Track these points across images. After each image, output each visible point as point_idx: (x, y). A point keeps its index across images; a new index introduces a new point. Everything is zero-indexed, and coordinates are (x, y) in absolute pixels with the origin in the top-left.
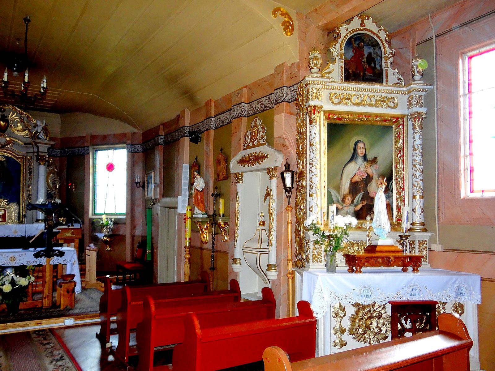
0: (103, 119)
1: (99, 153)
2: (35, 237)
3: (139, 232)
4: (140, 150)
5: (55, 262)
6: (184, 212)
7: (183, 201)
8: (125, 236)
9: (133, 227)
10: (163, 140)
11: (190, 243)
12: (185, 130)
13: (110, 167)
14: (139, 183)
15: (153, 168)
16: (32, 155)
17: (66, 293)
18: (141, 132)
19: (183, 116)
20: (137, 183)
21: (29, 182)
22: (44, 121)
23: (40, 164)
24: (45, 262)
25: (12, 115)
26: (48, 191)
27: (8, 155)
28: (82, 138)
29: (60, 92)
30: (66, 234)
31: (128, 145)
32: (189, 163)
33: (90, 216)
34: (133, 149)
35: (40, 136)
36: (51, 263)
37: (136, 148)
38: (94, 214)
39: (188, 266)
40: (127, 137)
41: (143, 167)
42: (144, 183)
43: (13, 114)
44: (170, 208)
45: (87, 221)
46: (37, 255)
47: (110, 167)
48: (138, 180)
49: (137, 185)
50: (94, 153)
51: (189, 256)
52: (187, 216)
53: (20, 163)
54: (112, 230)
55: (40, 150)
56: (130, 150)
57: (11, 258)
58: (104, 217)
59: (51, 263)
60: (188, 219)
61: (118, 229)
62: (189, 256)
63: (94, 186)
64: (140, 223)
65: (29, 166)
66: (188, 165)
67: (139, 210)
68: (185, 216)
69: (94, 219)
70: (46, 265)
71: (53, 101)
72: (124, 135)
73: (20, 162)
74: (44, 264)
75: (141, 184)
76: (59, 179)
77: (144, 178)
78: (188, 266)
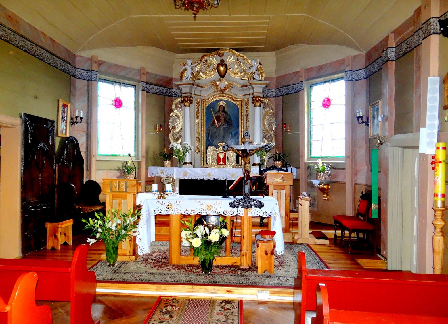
0: (316, 46)
1: (315, 89)
2: (235, 182)
3: (362, 179)
4: (362, 76)
5: (254, 213)
6: (431, 151)
7: (429, 135)
8: (344, 183)
9: (355, 173)
10: (393, 54)
11: (443, 202)
12: (432, 24)
13: (327, 103)
14: (362, 117)
15: (379, 96)
16: (248, 96)
17: (264, 254)
18: (364, 53)
19: (428, 4)
20: (358, 118)
21: (246, 125)
22: (258, 60)
23: (255, 106)
24: (243, 213)
25: (230, 59)
26: (264, 133)
27: (229, 99)
28: (297, 73)
29: (266, 18)
30: (276, 179)
31: (347, 72)
32: (439, 75)
33: (306, 159)
34: (353, 76)
35: (254, 77)
36: (249, 215)
37: (357, 74)
38: (311, 158)
39: (441, 239)
40: (346, 63)
41: (367, 97)
42: (368, 119)
43: (231, 57)
44: (405, 147)
45: (302, 166)
46: (233, 205)
47: (327, 103)
48: (359, 114)
49: (358, 120)
50: (309, 89)
51: (443, 223)
52: (437, 158)
53: (238, 106)
54: (330, 176)
55: (255, 91)
56: (350, 78)
57: (208, 206)
58: (320, 161)
59: (249, 215)
60: (440, 162)
61: (336, 176)
62: (443, 223)
63: (309, 127)
64: (363, 168)
65: (246, 109)
66: (438, 79)
67: (362, 153)
68: (433, 158)
69: (310, 163)
70: (244, 216)
71: (262, 34)
72: (342, 62)
73: (238, 105)
74: (242, 215)
75: (364, 119)
76: (275, 120)
77: (368, 111)
78: (439, 239)
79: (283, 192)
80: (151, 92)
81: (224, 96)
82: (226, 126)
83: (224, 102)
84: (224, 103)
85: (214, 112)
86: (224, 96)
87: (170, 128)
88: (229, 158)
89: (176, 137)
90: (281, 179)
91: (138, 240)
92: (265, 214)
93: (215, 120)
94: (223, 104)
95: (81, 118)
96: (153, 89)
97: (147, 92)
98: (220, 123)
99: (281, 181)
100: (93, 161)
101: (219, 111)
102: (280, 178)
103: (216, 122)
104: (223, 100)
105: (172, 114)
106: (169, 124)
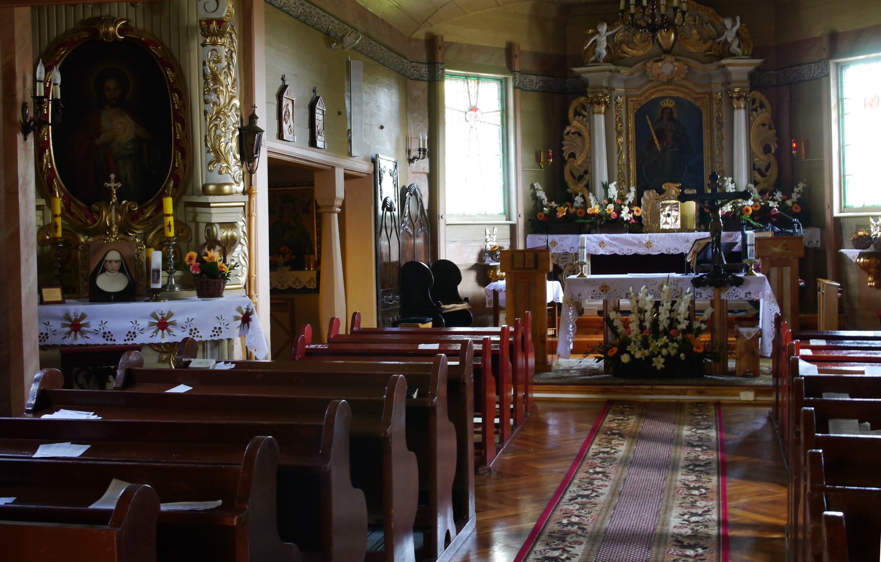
30: (773, 248)
79: (787, 270)
80: (529, 89)
81: (671, 90)
82: (676, 149)
83: (671, 101)
84: (672, 103)
85: (651, 122)
86: (671, 90)
87: (564, 158)
88: (443, 217)
89: (577, 175)
90: (782, 248)
91: (676, 251)
92: (748, 295)
93: (655, 138)
94: (670, 105)
95: (424, 150)
96: (532, 81)
97: (522, 90)
98: (665, 144)
99: (781, 250)
100: (442, 224)
101: (662, 118)
102: (781, 246)
103: (657, 142)
104: (670, 97)
105: (568, 129)
106: (564, 148)
